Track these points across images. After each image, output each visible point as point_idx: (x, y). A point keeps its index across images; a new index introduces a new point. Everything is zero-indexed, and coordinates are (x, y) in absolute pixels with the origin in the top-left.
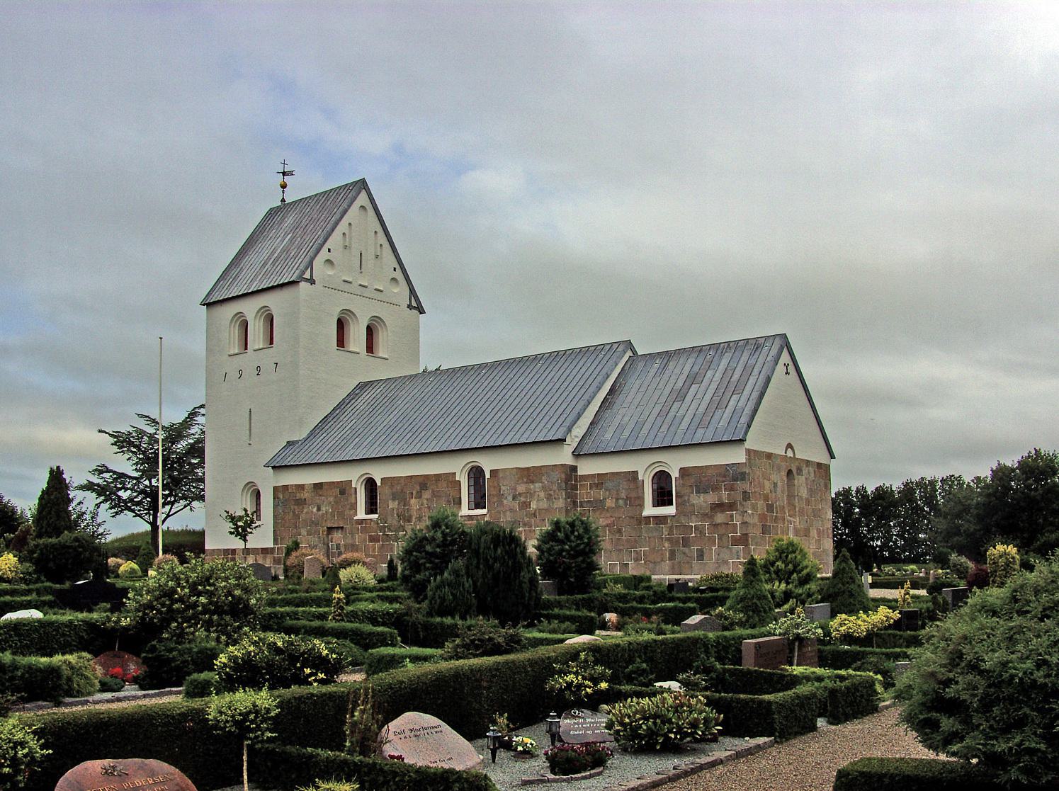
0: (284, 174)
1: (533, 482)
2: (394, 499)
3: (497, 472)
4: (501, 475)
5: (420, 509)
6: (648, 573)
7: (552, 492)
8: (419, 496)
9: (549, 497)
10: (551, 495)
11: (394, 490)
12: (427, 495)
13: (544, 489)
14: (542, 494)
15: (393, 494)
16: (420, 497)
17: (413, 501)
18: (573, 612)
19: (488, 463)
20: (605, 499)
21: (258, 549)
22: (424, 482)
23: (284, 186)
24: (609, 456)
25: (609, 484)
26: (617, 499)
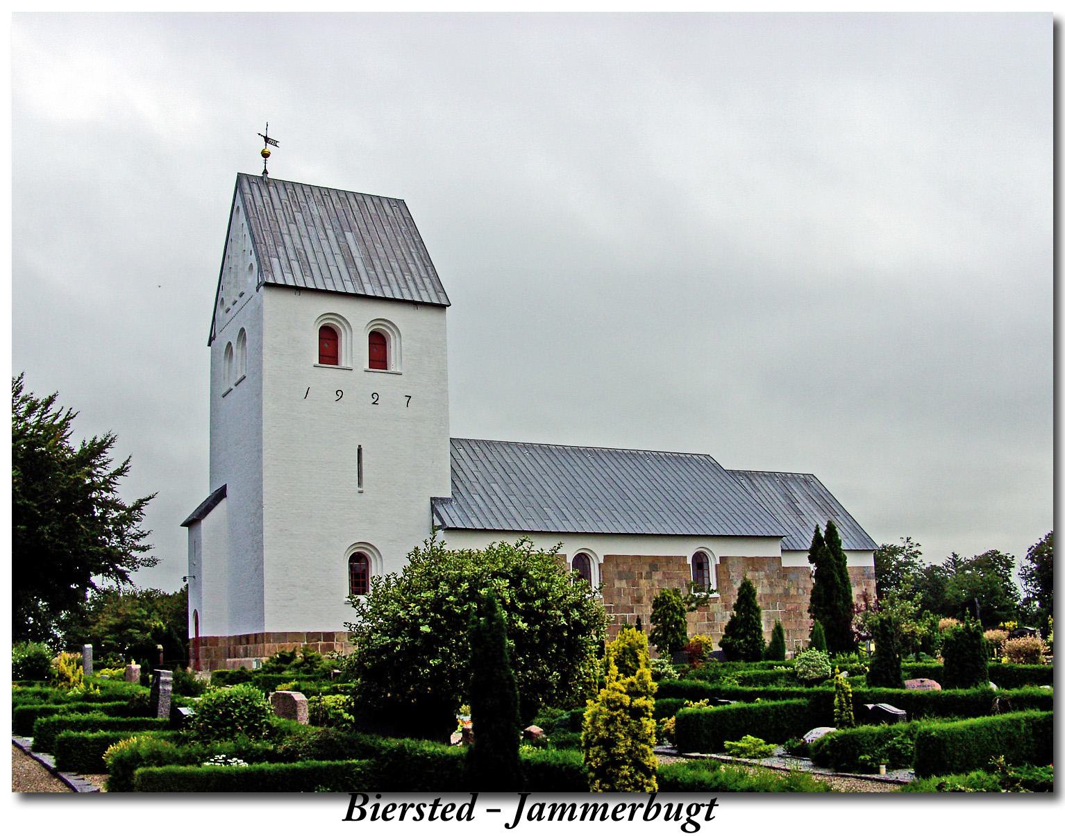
0: (267, 139)
1: (757, 570)
2: (620, 579)
3: (726, 560)
4: (730, 562)
5: (651, 590)
6: (310, 726)
7: (773, 580)
8: (649, 576)
9: (771, 585)
10: (772, 583)
11: (620, 569)
12: (657, 576)
13: (767, 576)
14: (765, 581)
15: (619, 573)
16: (651, 578)
17: (643, 582)
18: (762, 688)
19: (716, 551)
20: (789, 588)
21: (320, 633)
22: (654, 563)
23: (265, 155)
24: (546, 536)
25: (791, 576)
26: (798, 589)
